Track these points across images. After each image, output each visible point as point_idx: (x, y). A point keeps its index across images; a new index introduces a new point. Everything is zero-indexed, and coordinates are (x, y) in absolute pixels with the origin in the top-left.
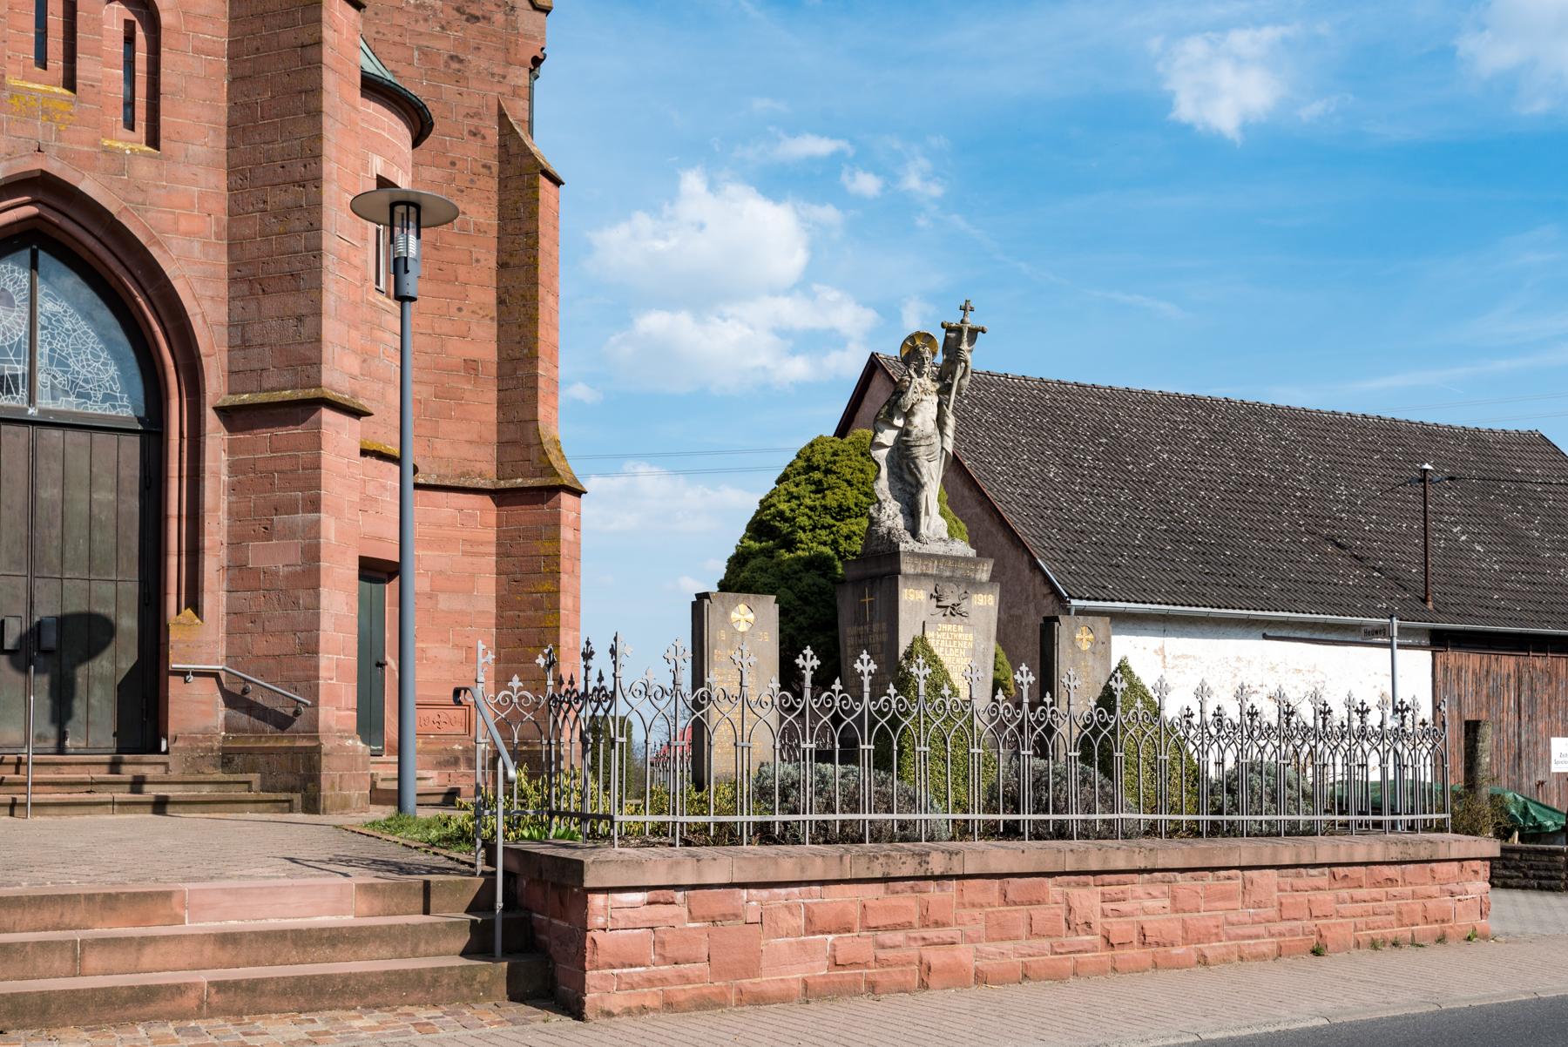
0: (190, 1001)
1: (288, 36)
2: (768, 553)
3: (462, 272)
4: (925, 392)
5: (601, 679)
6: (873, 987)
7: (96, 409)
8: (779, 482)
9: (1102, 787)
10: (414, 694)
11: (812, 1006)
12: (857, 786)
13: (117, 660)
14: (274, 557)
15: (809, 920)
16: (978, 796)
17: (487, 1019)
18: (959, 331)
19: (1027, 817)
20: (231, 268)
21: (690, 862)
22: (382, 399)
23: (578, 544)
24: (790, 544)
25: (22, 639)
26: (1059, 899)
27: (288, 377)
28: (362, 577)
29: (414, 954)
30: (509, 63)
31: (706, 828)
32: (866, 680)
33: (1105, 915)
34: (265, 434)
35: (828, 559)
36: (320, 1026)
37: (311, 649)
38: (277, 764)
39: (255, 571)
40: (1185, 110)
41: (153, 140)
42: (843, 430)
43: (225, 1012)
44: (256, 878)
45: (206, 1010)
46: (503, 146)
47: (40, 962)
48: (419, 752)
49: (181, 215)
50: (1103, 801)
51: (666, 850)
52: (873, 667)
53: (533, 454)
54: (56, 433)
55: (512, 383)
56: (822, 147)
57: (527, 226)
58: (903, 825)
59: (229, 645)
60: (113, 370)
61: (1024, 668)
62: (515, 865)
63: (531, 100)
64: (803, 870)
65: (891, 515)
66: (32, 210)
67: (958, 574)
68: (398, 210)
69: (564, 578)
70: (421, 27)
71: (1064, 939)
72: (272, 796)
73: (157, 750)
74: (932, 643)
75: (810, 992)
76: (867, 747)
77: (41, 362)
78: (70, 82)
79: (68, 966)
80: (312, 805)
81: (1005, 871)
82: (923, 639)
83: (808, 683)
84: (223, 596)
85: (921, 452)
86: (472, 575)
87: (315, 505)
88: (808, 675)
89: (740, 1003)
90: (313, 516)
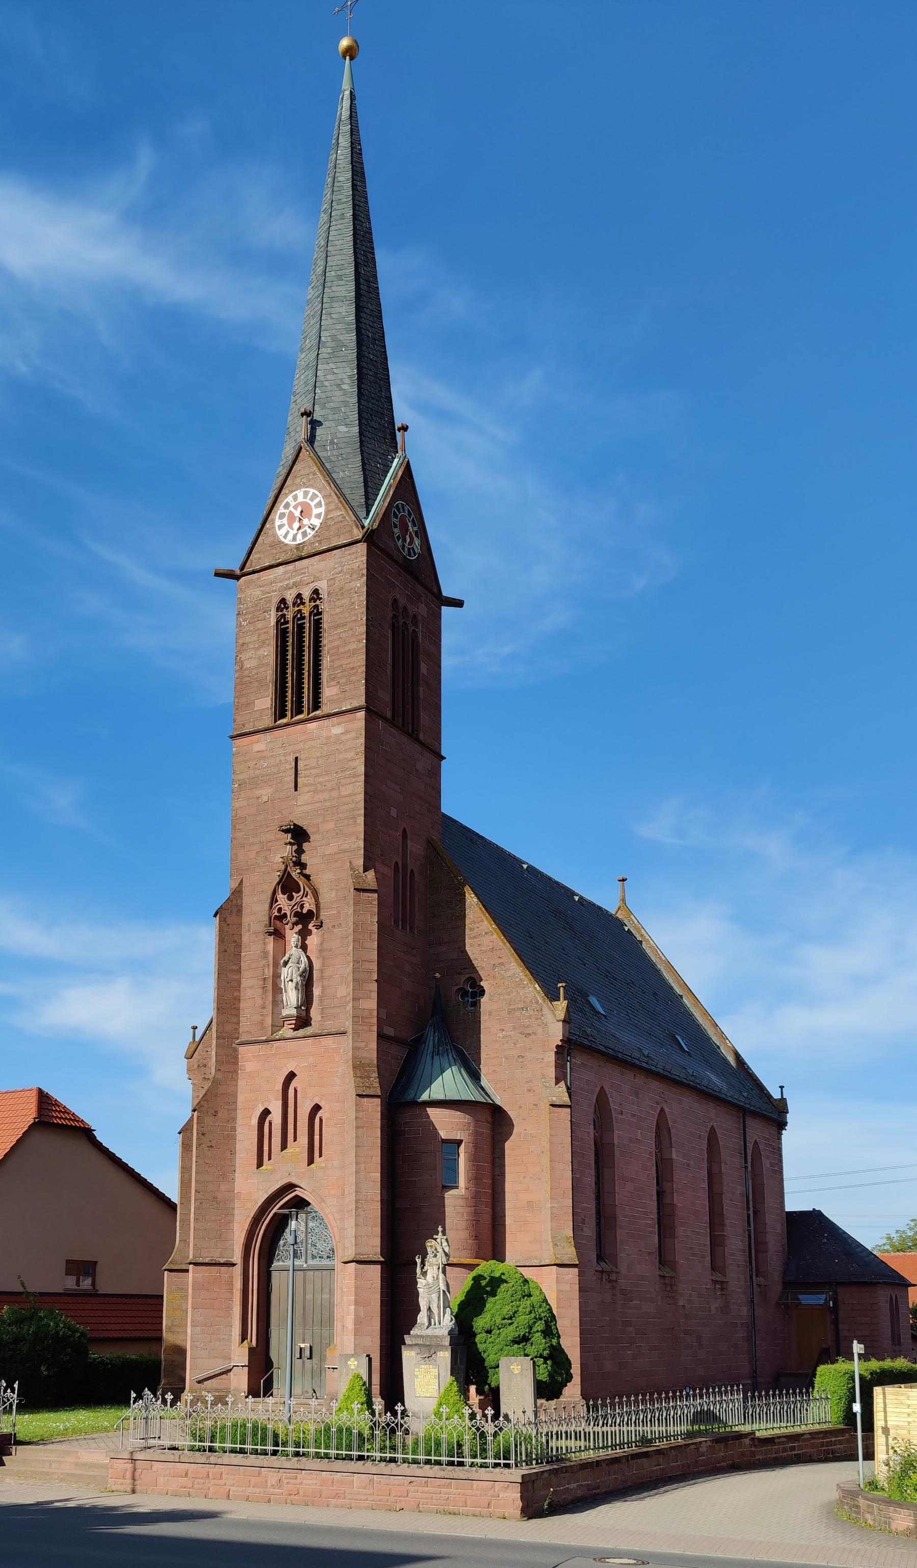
54: (312, 1273)
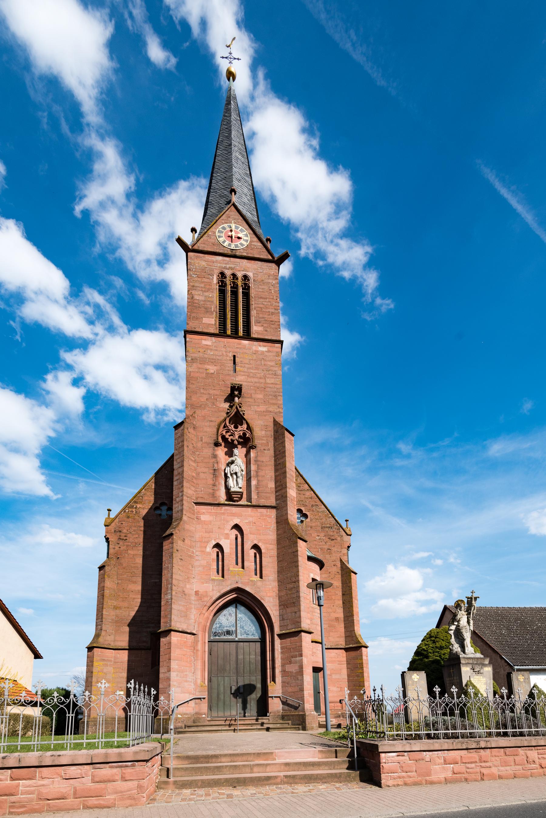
0: (279, 780)
1: (290, 551)
2: (421, 660)
3: (333, 597)
4: (463, 615)
5: (379, 696)
6: (466, 780)
7: (250, 637)
8: (422, 641)
9: (533, 721)
10: (329, 699)
11: (448, 785)
12: (455, 723)
13: (257, 694)
14: (292, 668)
15: (445, 761)
16: (493, 724)
17: (355, 787)
18: (471, 598)
19: (510, 730)
20: (279, 603)
21: (408, 745)
22: (316, 629)
23: (367, 660)
24: (427, 657)
25: (235, 690)
26: (523, 754)
27: (294, 626)
28: (313, 672)
29: (334, 769)
30: (342, 548)
31: (411, 735)
32: (455, 693)
33: (539, 758)
34: (289, 640)
35: (438, 660)
36: (311, 788)
37: (302, 690)
38: (295, 719)
39: (288, 672)
40: (533, 530)
41: (261, 577)
42: (438, 626)
43: (287, 783)
44: (293, 748)
45: (282, 783)
46: (342, 567)
47: (243, 770)
48: (331, 714)
49: (268, 593)
50: (534, 725)
51: (401, 741)
52: (456, 690)
53: (354, 638)
54: (242, 643)
55: (347, 622)
56: (426, 554)
57: (349, 585)
58: (470, 733)
59: (282, 690)
60: (254, 628)
61: (504, 688)
62: (359, 745)
63: (348, 556)
64: (441, 746)
65: (456, 648)
66: (236, 595)
67: (479, 662)
68: (317, 585)
69: (365, 669)
70: (321, 544)
71: (526, 766)
72: (294, 726)
73: (266, 716)
74: (473, 682)
75: (447, 781)
76: (457, 712)
77: (238, 628)
78: (243, 567)
79: (250, 771)
80: (304, 729)
81: (505, 746)
82: (470, 681)
83: (437, 695)
84: (280, 678)
85: (463, 631)
86: (341, 669)
87: (301, 655)
88: (437, 693)
89: (426, 784)
90: (301, 658)
